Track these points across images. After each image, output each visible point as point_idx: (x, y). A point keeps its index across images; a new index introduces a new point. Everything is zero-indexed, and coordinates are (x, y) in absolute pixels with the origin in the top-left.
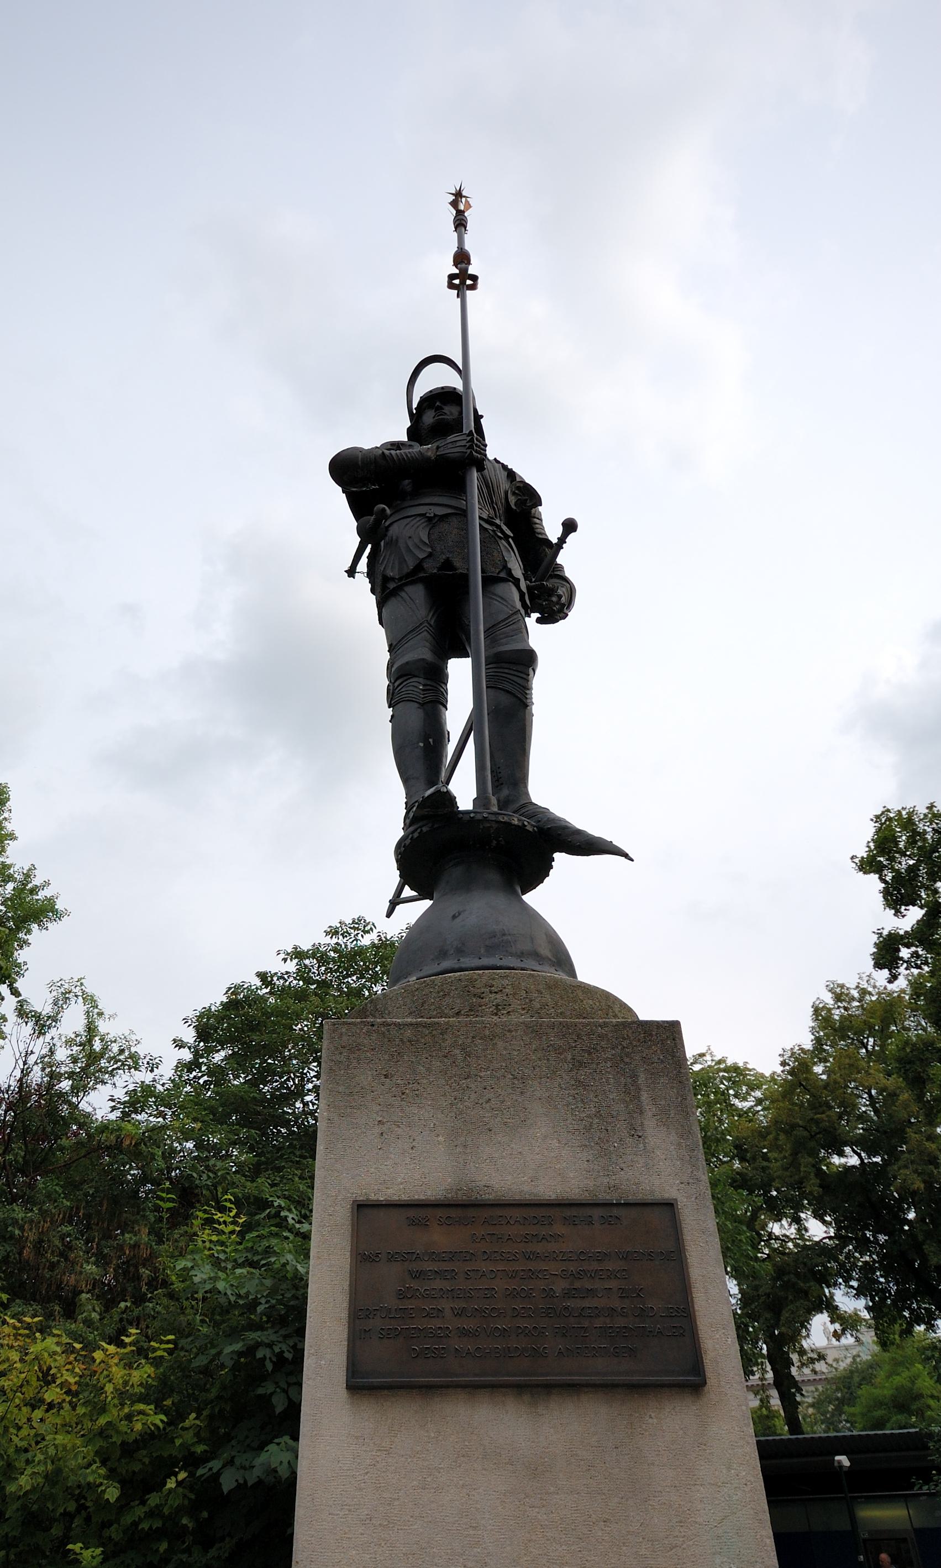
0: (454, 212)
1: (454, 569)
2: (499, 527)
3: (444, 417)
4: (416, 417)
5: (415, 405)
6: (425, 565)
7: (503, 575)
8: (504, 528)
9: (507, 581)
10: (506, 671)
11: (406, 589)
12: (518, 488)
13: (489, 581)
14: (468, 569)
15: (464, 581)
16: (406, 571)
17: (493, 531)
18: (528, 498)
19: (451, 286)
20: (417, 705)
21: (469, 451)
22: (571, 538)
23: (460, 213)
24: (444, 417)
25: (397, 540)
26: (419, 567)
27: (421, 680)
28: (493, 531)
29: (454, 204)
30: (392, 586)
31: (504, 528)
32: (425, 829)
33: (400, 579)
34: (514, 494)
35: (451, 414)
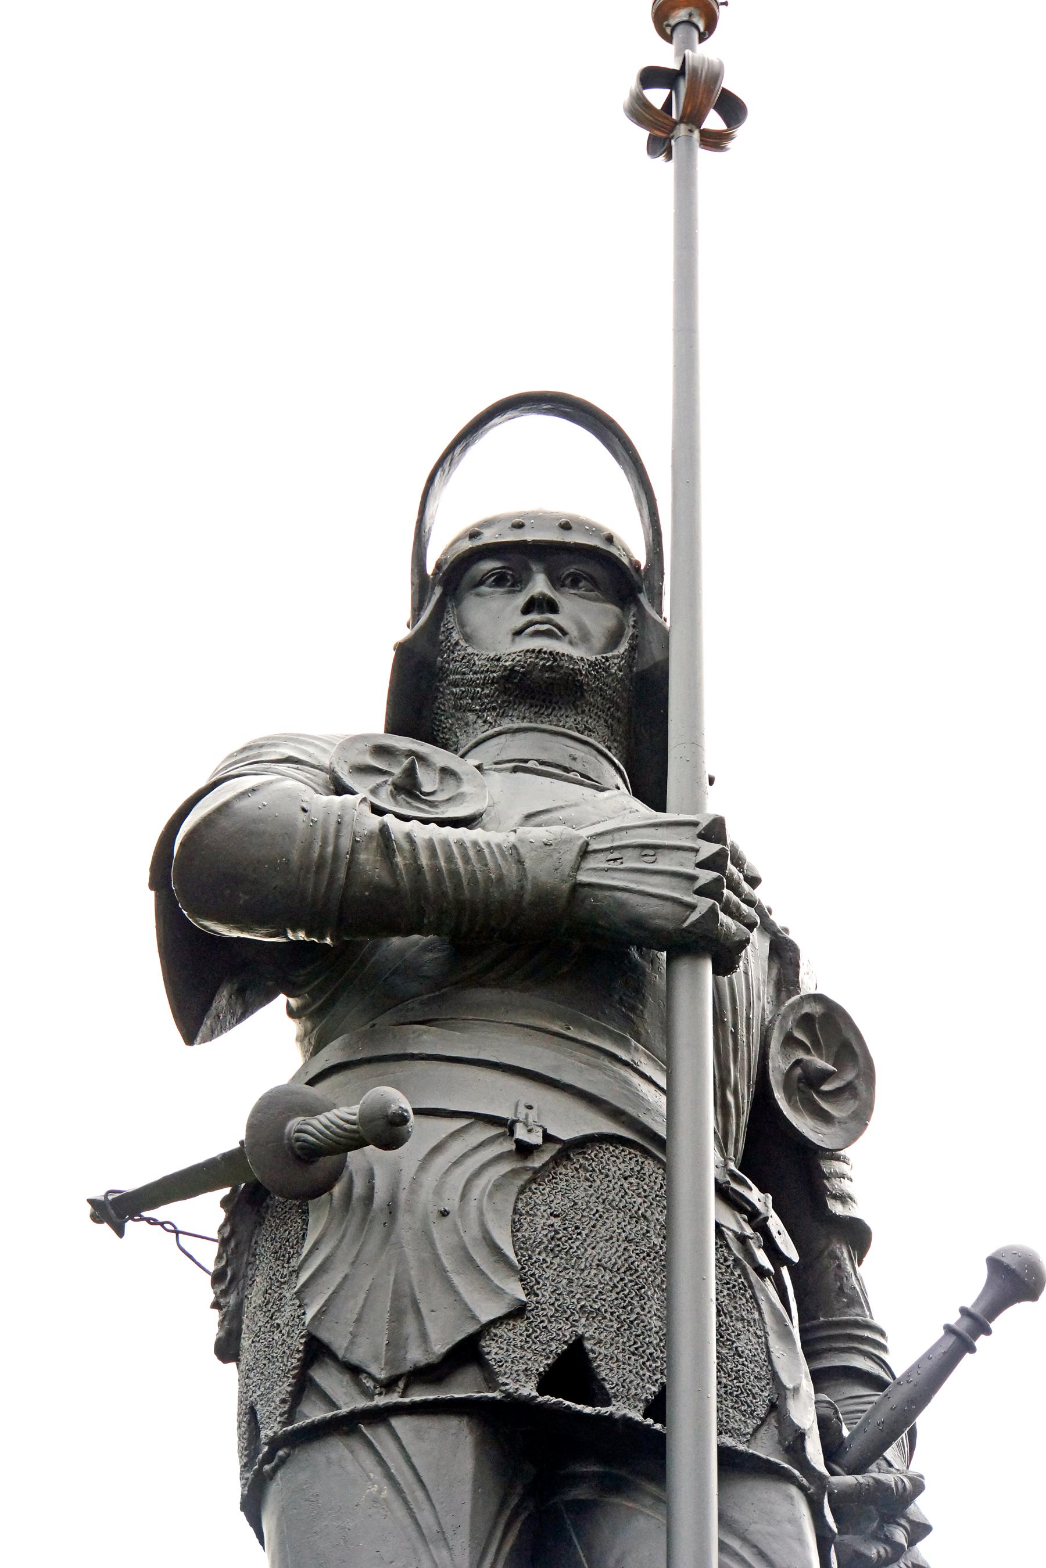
1: (596, 1393)
2: (754, 1217)
3: (554, 636)
6: (492, 1350)
7: (765, 1448)
8: (775, 1224)
9: (787, 1477)
12: (806, 1021)
13: (734, 1464)
14: (658, 1407)
15: (639, 1454)
16: (415, 1356)
17: (742, 1239)
18: (829, 1055)
19: (639, 111)
21: (704, 904)
22: (1016, 1316)
24: (554, 636)
25: (392, 1208)
26: (468, 1353)
28: (742, 1239)
30: (348, 1400)
31: (775, 1224)
35: (585, 637)
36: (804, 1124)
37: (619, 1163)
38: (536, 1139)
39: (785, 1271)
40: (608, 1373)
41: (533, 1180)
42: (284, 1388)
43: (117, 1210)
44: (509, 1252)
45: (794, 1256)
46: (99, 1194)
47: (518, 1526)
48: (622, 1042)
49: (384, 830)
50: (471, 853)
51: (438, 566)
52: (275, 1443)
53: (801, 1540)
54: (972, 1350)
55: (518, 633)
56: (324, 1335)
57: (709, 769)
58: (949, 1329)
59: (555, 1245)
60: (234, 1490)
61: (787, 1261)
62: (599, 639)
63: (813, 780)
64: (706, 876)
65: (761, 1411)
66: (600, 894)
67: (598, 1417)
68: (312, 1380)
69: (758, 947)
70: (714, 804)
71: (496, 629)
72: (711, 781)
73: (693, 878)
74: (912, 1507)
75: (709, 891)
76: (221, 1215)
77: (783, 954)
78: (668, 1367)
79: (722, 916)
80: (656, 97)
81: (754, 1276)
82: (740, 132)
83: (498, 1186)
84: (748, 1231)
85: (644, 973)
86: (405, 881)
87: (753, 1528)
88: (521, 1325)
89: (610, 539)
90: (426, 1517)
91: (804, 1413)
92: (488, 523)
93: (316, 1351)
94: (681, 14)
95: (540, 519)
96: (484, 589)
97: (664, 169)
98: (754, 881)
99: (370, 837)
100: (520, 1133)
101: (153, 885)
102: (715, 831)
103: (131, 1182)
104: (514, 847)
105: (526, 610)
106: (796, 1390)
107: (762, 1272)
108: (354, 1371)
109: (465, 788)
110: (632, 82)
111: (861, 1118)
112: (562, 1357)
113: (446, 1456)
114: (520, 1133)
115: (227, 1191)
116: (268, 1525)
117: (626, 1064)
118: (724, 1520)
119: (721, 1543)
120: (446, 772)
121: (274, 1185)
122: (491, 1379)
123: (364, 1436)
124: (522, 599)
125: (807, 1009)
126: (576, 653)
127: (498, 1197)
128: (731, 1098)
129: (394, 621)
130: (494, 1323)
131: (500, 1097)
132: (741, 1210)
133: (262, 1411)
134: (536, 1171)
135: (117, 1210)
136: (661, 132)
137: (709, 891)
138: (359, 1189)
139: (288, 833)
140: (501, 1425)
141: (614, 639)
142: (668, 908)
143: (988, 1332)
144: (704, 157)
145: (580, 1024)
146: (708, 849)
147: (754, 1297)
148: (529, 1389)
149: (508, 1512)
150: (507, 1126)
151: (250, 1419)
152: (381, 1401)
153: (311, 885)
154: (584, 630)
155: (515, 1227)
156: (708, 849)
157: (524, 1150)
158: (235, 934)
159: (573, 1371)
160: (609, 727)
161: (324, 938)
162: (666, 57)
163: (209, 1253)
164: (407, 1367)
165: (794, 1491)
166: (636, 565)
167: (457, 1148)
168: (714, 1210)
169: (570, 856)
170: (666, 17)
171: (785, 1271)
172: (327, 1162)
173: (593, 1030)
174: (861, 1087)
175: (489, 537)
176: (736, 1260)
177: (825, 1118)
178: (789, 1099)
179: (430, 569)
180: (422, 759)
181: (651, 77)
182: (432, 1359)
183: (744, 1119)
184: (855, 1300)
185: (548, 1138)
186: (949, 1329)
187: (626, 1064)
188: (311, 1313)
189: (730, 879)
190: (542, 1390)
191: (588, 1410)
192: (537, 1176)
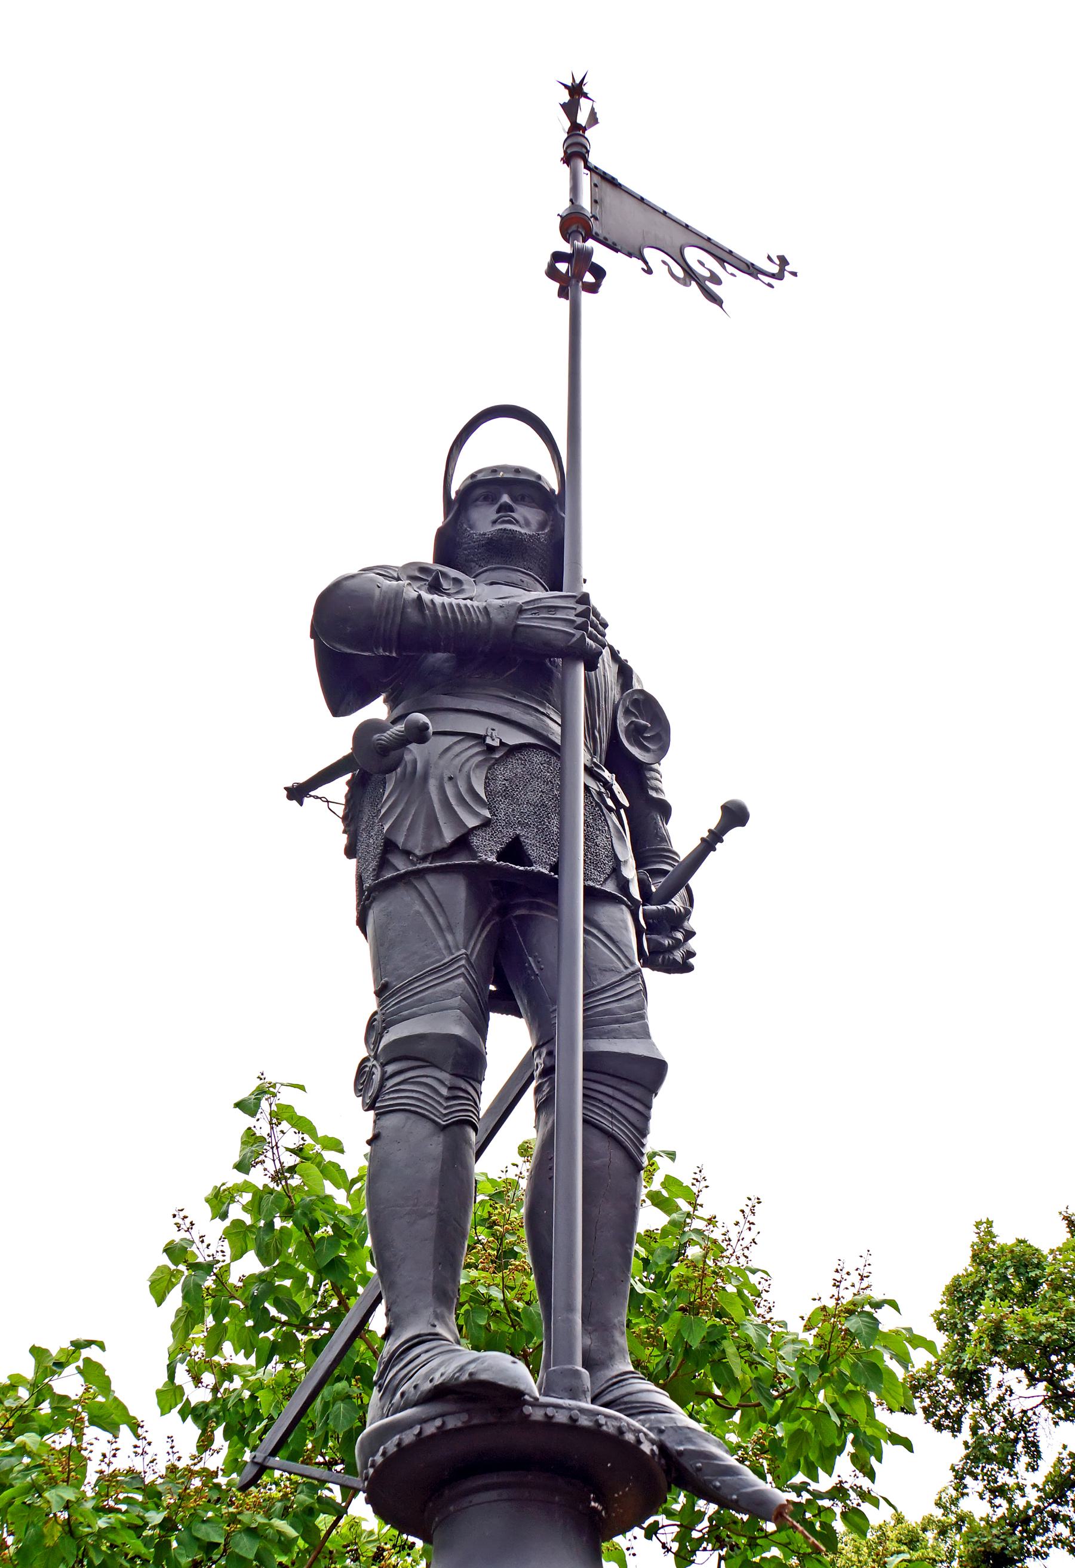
0: (567, 124)
1: (525, 860)
3: (511, 521)
4: (459, 505)
5: (456, 486)
6: (476, 841)
7: (610, 887)
8: (617, 788)
9: (621, 902)
10: (610, 1091)
11: (431, 879)
12: (635, 703)
13: (593, 895)
14: (555, 868)
15: (548, 889)
16: (437, 845)
17: (600, 793)
18: (649, 721)
19: (552, 273)
20: (428, 1127)
21: (578, 634)
22: (734, 835)
23: (576, 129)
24: (511, 521)
26: (463, 843)
27: (445, 1076)
28: (600, 793)
29: (570, 109)
30: (402, 866)
31: (617, 788)
32: (452, 1423)
33: (424, 859)
34: (627, 712)
35: (527, 524)
36: (635, 751)
37: (538, 758)
38: (496, 743)
39: (622, 811)
40: (533, 853)
41: (494, 765)
42: (374, 864)
43: (298, 793)
44: (484, 796)
45: (627, 804)
46: (290, 785)
47: (488, 929)
48: (544, 706)
49: (419, 597)
50: (464, 610)
51: (457, 493)
52: (371, 890)
53: (627, 929)
54: (715, 850)
55: (494, 522)
56: (393, 838)
57: (584, 577)
58: (703, 839)
59: (506, 794)
60: (353, 914)
61: (623, 806)
62: (534, 525)
63: (635, 582)
64: (579, 620)
65: (608, 871)
66: (528, 630)
67: (526, 871)
68: (388, 861)
69: (606, 652)
70: (585, 588)
71: (484, 521)
72: (585, 581)
73: (573, 621)
74: (686, 923)
75: (583, 627)
76: (346, 789)
77: (625, 672)
78: (560, 852)
79: (588, 640)
80: (562, 267)
81: (605, 811)
82: (605, 282)
83: (478, 766)
84: (603, 790)
85: (552, 672)
86: (430, 621)
87: (603, 923)
88: (489, 830)
89: (539, 477)
90: (441, 920)
91: (630, 872)
92: (480, 471)
93: (389, 846)
94: (574, 228)
95: (505, 468)
96: (479, 503)
97: (565, 304)
98: (605, 625)
99: (413, 600)
100: (489, 741)
101: (312, 637)
102: (584, 599)
103: (302, 779)
104: (485, 608)
105: (498, 512)
106: (626, 862)
107: (610, 809)
108: (407, 853)
109: (464, 587)
110: (548, 259)
111: (663, 750)
112: (509, 845)
113: (455, 893)
114: (489, 741)
115: (348, 776)
116: (370, 929)
117: (543, 714)
118: (587, 920)
119: (585, 929)
120: (457, 581)
121: (369, 768)
122: (473, 854)
123: (415, 887)
124: (496, 506)
125: (636, 697)
126: (523, 531)
127: (478, 771)
128: (597, 734)
129: (437, 519)
130: (475, 828)
131: (478, 726)
132: (600, 781)
133: (365, 876)
134: (497, 760)
135: (298, 793)
136: (568, 287)
137: (583, 627)
138: (409, 769)
139: (370, 597)
140: (478, 876)
141: (542, 526)
142: (560, 636)
143: (722, 841)
144: (585, 296)
145: (521, 695)
146: (581, 608)
147: (605, 820)
148: (492, 859)
149: (483, 919)
150: (481, 739)
151: (360, 880)
152: (420, 866)
153: (383, 625)
154: (527, 521)
155: (487, 785)
156: (581, 608)
157: (491, 749)
158: (349, 651)
159: (514, 851)
160: (541, 568)
161: (391, 652)
162: (566, 248)
163: (340, 810)
164: (432, 850)
165: (624, 907)
166: (553, 491)
167: (457, 749)
168: (582, 778)
169: (513, 612)
170: (567, 229)
171: (622, 811)
172: (394, 754)
173: (526, 698)
174: (663, 735)
175: (480, 477)
176: (597, 803)
177: (646, 749)
178: (631, 743)
179: (453, 496)
180: (444, 575)
181: (557, 257)
182: (445, 846)
183: (604, 745)
184: (664, 839)
185: (501, 743)
186: (703, 839)
187: (543, 714)
188: (386, 828)
189: (592, 622)
190: (498, 860)
191: (522, 868)
192: (497, 761)
